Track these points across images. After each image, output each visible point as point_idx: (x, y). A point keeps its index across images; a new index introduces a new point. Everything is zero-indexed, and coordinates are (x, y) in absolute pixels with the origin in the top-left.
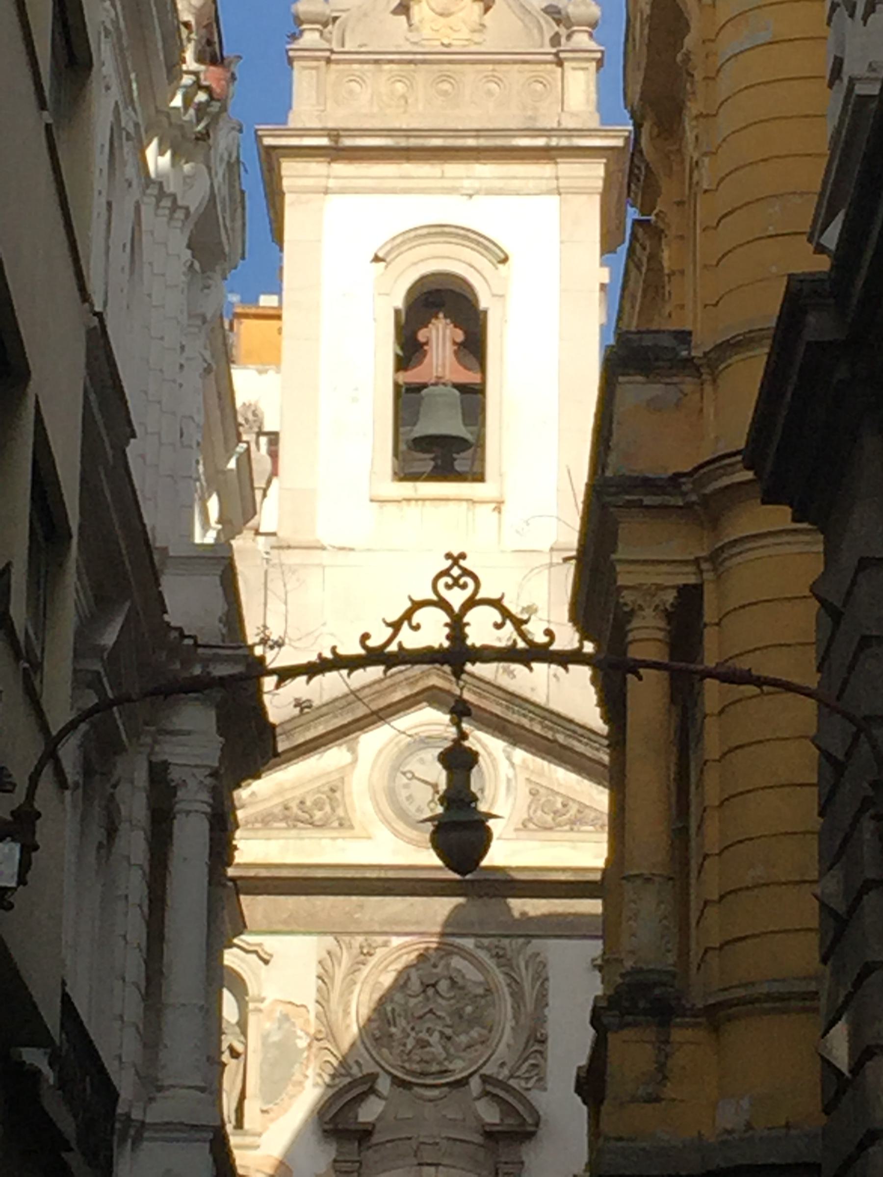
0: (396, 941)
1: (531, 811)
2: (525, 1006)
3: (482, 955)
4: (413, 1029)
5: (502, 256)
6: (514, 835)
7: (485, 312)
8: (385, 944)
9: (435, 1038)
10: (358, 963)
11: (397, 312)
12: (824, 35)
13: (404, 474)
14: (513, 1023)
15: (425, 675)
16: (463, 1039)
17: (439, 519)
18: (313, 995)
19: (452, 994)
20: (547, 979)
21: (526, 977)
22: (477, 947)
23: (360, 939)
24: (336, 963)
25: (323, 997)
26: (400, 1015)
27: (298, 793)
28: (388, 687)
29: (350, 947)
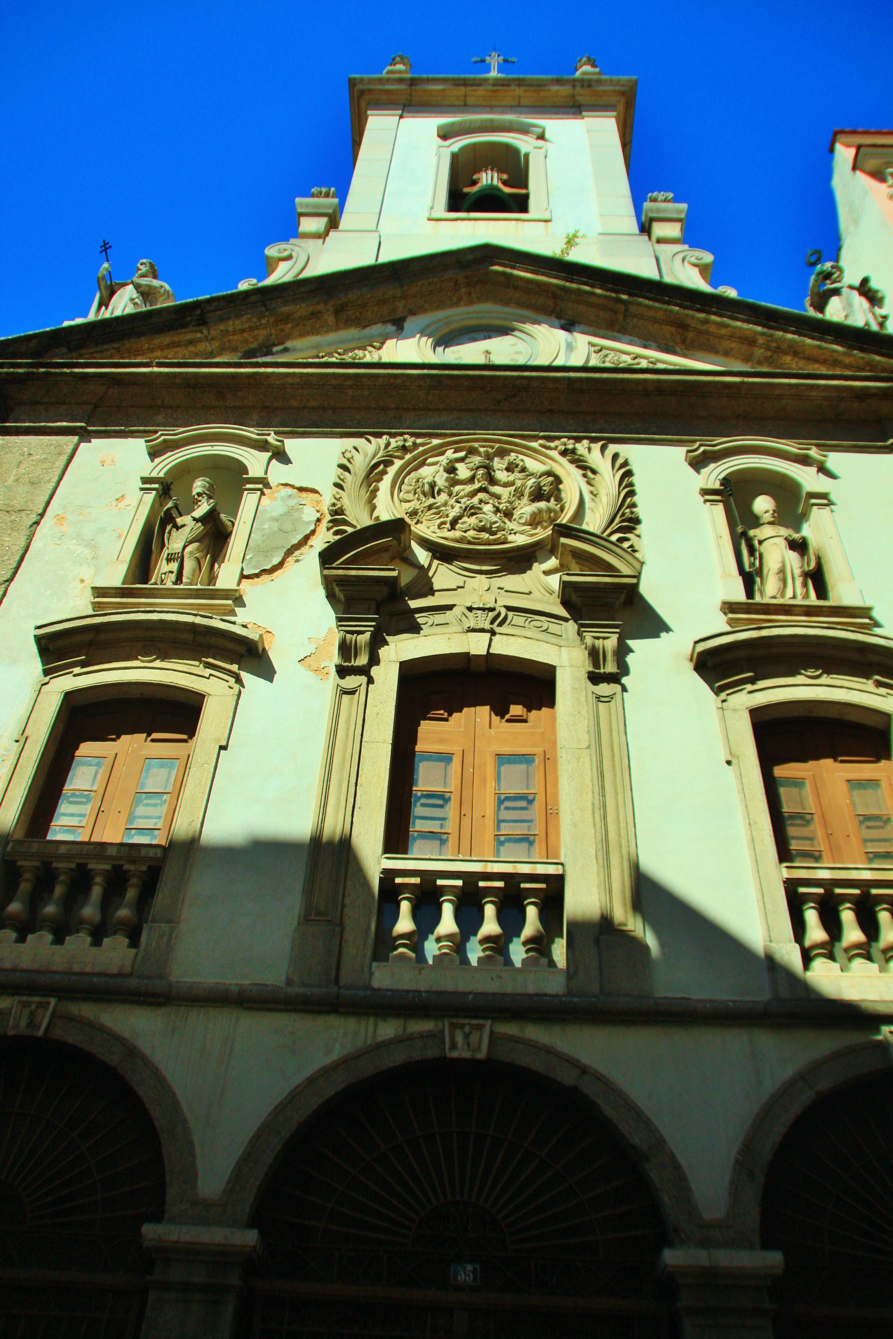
5: (539, 130)
9: (488, 508)
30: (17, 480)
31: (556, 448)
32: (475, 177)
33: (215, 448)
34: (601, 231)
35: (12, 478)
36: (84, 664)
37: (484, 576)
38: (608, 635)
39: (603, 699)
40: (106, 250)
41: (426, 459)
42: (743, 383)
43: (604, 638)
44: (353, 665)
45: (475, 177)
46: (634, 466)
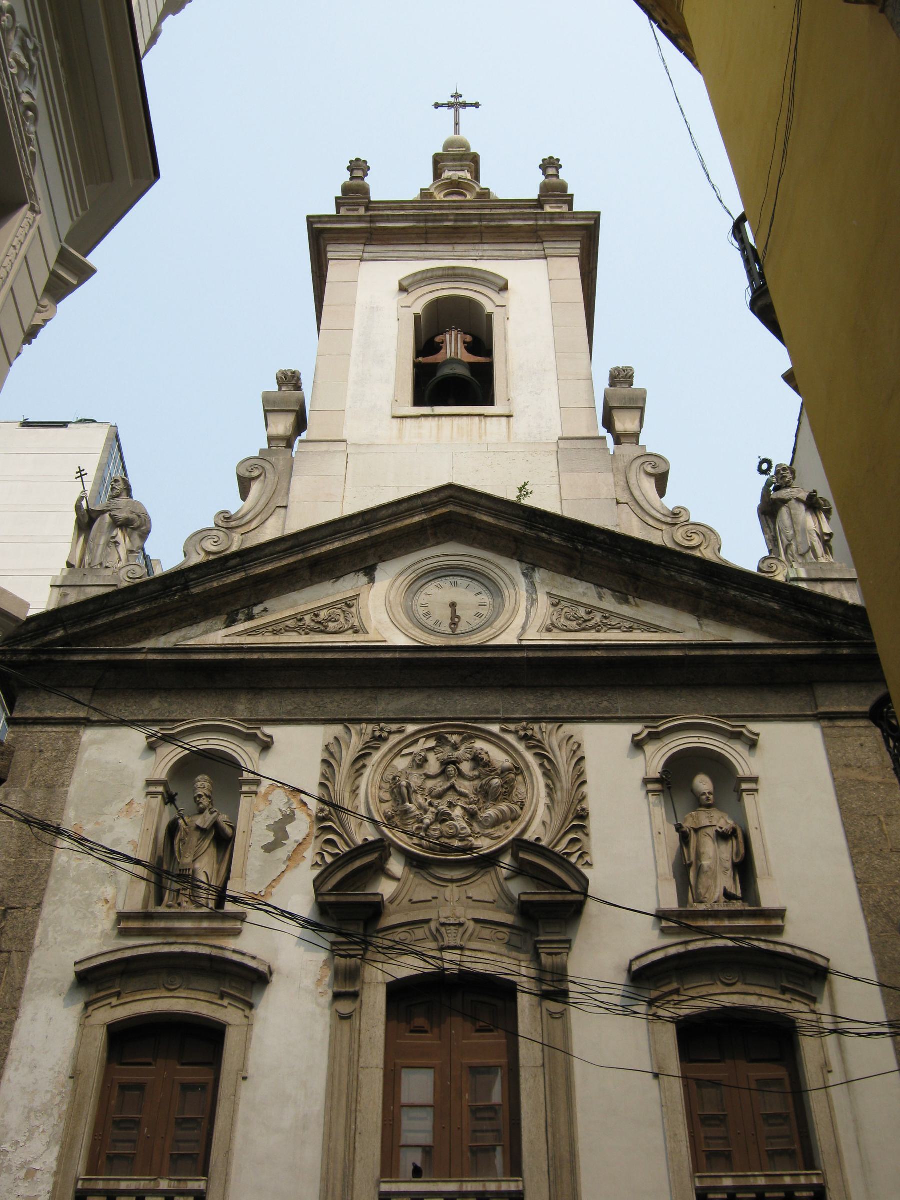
0: (411, 728)
1: (554, 618)
2: (561, 782)
3: (511, 738)
4: (431, 804)
5: (502, 283)
6: (358, 1002)
7: (490, 317)
9: (458, 812)
10: (369, 748)
11: (417, 318)
13: (418, 401)
14: (548, 801)
16: (492, 812)
18: (317, 778)
19: (476, 773)
21: (562, 759)
22: (503, 730)
24: (343, 747)
25: (332, 754)
26: (415, 792)
28: (407, 511)
29: (361, 734)
30: (33, 783)
31: (516, 733)
32: (438, 339)
33: (211, 742)
34: (560, 435)
35: (29, 781)
36: (118, 995)
37: (455, 885)
38: (560, 951)
39: (555, 1016)
40: (82, 476)
41: (401, 751)
42: (686, 656)
43: (556, 954)
44: (345, 989)
45: (438, 339)
46: (588, 751)
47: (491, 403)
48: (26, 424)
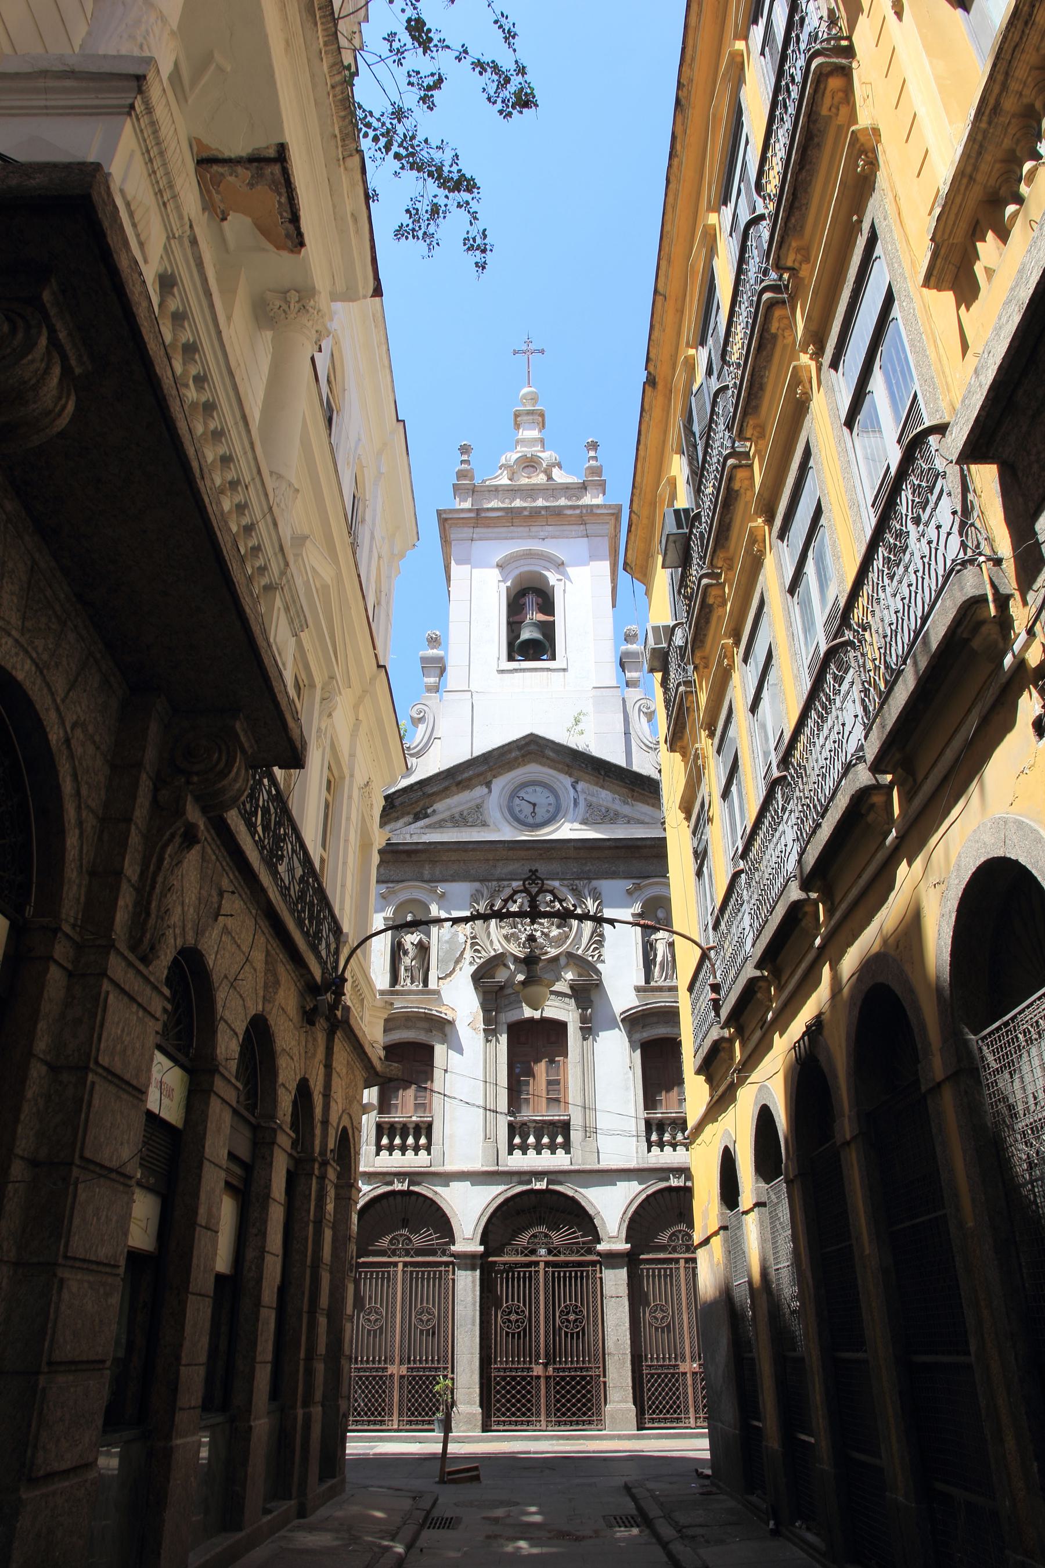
8: (509, 886)
12: (642, 765)
13: (511, 658)
15: (841, 582)
17: (532, 680)
20: (453, 1404)
23: (494, 883)
27: (458, 809)
45: (522, 601)
47: (553, 658)
48: (907, 141)
